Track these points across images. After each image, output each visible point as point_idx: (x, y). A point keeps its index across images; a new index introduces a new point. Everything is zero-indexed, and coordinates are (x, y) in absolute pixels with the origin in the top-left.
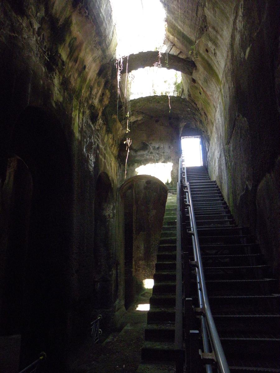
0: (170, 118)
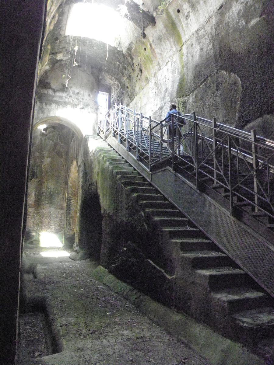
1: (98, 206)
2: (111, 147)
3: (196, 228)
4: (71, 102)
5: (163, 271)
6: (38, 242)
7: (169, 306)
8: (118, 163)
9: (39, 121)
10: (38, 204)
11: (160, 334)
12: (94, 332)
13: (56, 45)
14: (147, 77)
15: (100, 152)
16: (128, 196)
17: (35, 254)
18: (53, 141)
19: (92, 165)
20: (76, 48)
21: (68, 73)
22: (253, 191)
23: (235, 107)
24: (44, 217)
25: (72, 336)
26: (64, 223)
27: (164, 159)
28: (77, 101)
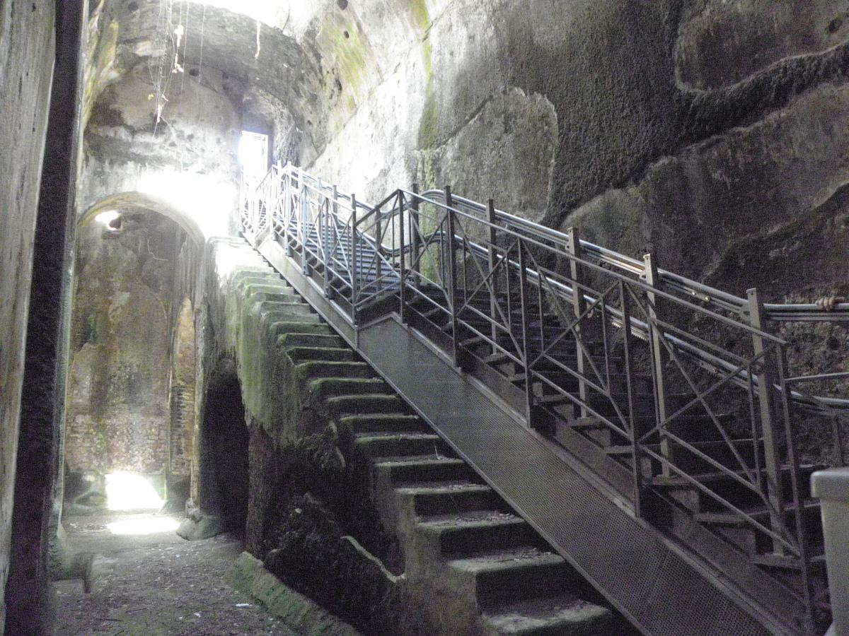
0: (225, 76)
1: (240, 409)
2: (270, 265)
4: (175, 157)
6: (100, 498)
8: (283, 305)
9: (96, 204)
13: (133, 20)
14: (353, 100)
16: (302, 384)
17: (92, 528)
18: (135, 251)
20: (179, 31)
21: (162, 88)
22: (576, 369)
23: (546, 175)
26: (166, 447)
28: (189, 156)
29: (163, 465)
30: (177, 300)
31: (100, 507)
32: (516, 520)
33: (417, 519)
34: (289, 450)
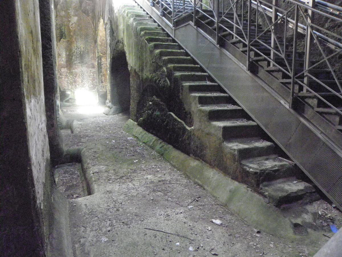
1: (126, 64)
2: (136, 2)
3: (224, 93)
5: (183, 123)
6: (73, 100)
7: (188, 154)
8: (142, 19)
10: (70, 64)
11: (179, 178)
12: (122, 177)
15: (124, 8)
16: (151, 52)
17: (72, 111)
19: (117, 22)
22: (270, 46)
24: (77, 77)
25: (102, 181)
27: (187, 14)
29: (96, 87)
30: (97, 20)
31: (74, 103)
32: (239, 108)
33: (199, 105)
34: (147, 79)
